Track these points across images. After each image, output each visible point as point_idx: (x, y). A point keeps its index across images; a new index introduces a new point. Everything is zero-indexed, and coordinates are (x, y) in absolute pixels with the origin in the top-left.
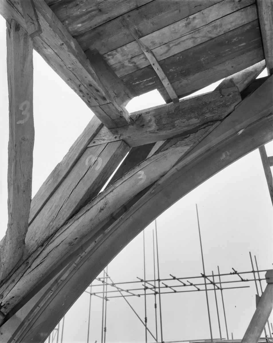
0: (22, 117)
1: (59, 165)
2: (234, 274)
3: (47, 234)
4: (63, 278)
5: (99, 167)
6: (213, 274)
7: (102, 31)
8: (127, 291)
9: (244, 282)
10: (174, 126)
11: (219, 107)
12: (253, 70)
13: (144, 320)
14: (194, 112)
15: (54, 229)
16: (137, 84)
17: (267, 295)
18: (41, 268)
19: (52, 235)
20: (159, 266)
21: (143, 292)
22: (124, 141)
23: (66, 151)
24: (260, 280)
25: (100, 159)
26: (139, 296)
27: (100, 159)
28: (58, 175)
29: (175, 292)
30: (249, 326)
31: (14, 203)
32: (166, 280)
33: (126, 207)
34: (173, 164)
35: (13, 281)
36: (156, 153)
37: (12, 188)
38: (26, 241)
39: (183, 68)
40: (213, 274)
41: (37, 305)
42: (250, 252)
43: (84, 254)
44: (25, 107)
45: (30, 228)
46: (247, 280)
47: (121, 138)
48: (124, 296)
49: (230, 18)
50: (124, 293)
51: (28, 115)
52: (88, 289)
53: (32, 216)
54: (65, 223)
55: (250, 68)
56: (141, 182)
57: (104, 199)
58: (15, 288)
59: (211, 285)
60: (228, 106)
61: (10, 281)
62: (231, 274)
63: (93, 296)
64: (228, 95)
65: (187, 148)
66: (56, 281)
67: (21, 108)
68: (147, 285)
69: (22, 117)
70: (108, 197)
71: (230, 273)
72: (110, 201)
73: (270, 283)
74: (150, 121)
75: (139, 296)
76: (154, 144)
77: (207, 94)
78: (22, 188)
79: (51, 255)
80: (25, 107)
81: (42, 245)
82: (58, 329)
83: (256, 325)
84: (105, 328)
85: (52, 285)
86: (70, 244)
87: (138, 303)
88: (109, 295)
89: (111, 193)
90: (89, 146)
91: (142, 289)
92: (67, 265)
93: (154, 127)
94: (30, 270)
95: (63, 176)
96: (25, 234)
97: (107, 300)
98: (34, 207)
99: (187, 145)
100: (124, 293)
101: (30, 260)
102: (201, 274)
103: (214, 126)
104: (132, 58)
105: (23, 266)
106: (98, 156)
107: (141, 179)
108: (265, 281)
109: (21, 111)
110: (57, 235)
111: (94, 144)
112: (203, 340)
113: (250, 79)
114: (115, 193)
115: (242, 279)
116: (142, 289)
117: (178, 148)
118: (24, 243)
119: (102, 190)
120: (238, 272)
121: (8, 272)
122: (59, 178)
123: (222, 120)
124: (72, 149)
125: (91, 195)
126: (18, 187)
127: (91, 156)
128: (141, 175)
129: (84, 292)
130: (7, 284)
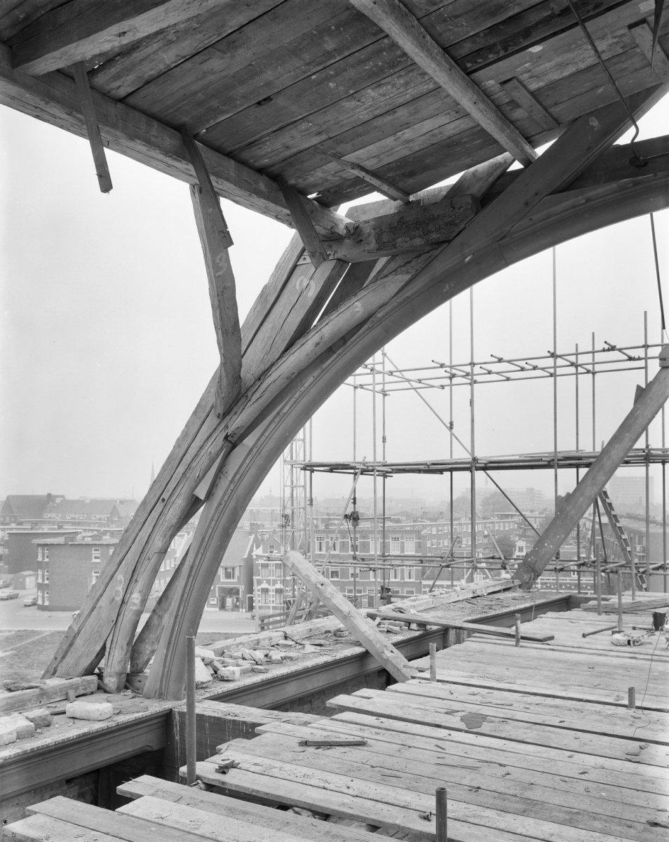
0: (219, 269)
1: (265, 287)
2: (609, 350)
3: (263, 368)
4: (284, 411)
5: (312, 293)
8: (420, 381)
10: (395, 246)
11: (446, 224)
12: (502, 161)
13: (449, 425)
14: (418, 229)
15: (270, 363)
16: (350, 192)
17: (656, 386)
18: (260, 401)
19: (268, 369)
21: (447, 382)
22: (339, 260)
23: (271, 269)
25: (312, 283)
26: (443, 387)
27: (312, 283)
28: (266, 300)
29: (508, 379)
30: (616, 432)
31: (224, 345)
33: (343, 340)
34: (392, 295)
35: (236, 413)
36: (372, 282)
37: (220, 331)
38: (242, 376)
39: (401, 176)
41: (262, 434)
42: (645, 313)
43: (303, 388)
44: (221, 260)
45: (244, 360)
46: (639, 357)
47: (336, 257)
48: (415, 389)
49: (452, 125)
50: (416, 385)
51: (226, 265)
52: (350, 380)
53: (244, 348)
54: (280, 357)
55: (499, 158)
56: (359, 315)
57: (320, 332)
59: (571, 367)
60: (456, 225)
61: (232, 413)
62: (604, 350)
63: (359, 390)
64: (461, 207)
65: (407, 277)
66: (278, 413)
67: (218, 261)
68: (454, 371)
69: (219, 269)
70: (323, 330)
71: (601, 349)
72: (326, 336)
73: (666, 367)
74: (369, 235)
75: (443, 387)
76: (375, 262)
77: (350, 331)
78: (230, 330)
79: (270, 389)
80: (221, 260)
81: (259, 379)
82: (304, 440)
83: (628, 431)
85: (275, 417)
86: (288, 378)
87: (438, 398)
88: (387, 387)
89: (327, 326)
90: (298, 264)
92: (335, 290)
93: (373, 245)
95: (272, 301)
96: (240, 370)
97: (385, 395)
98: (246, 336)
99: (408, 273)
100: (416, 385)
101: (249, 394)
102: (549, 352)
103: (439, 250)
104: (335, 173)
105: (243, 399)
106: (311, 279)
107: (358, 312)
108: (658, 360)
109: (218, 263)
110: (274, 369)
111: (304, 262)
112: (546, 453)
113: (499, 172)
114: (327, 329)
115: (628, 356)
117: (398, 276)
118: (241, 378)
119: (315, 323)
120: (618, 347)
121: (228, 405)
122: (270, 301)
123: (449, 242)
124: (278, 267)
125: (303, 329)
126: (226, 331)
127: (302, 277)
128: (356, 307)
129: (342, 385)
130: (230, 417)
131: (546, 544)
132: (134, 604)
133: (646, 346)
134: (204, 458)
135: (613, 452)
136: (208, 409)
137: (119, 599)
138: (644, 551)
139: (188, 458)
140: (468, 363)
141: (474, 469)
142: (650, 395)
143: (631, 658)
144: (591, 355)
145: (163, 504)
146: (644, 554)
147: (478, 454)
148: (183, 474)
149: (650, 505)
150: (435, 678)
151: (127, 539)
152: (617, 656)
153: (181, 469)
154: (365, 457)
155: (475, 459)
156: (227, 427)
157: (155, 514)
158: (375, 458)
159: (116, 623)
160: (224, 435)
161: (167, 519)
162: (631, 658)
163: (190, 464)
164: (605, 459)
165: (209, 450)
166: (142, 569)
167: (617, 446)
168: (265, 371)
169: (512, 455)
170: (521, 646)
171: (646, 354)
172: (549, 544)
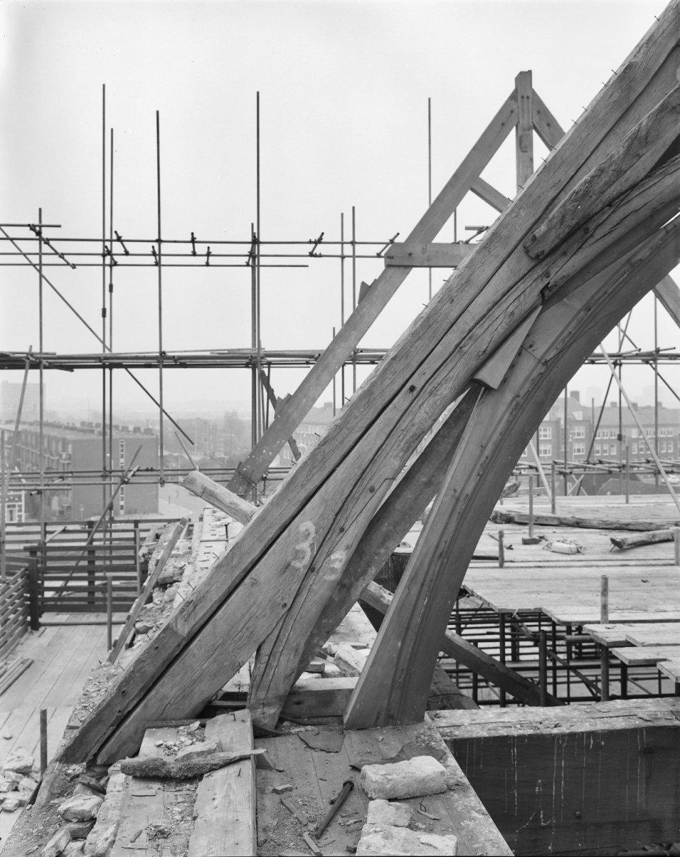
6: (101, 265)
7: (89, 405)
9: (313, 258)
17: (381, 284)
19: (627, 191)
20: (144, 392)
24: (209, 254)
32: (664, 381)
40: (101, 265)
58: (570, 263)
83: (354, 329)
84: (111, 287)
91: (214, 255)
94: (592, 240)
101: (592, 226)
110: (636, 193)
112: (225, 350)
115: (63, 258)
116: (214, 255)
131: (264, 451)
132: (333, 570)
133: (353, 243)
134: (499, 321)
135: (339, 350)
136: (514, 243)
137: (301, 565)
138: (70, 459)
139: (467, 321)
140: (155, 239)
141: (161, 366)
142: (376, 294)
143: (622, 566)
144: (340, 245)
145: (411, 397)
146: (69, 462)
147: (661, 346)
148: (457, 346)
149: (44, 413)
150: (607, 619)
151: (324, 460)
152: (609, 566)
153: (453, 338)
154: (31, 347)
155: (162, 353)
156: (547, 274)
157: (391, 414)
158: (41, 349)
159: (290, 609)
160: (541, 286)
161: (416, 421)
162: (622, 566)
163: (470, 331)
164: (330, 358)
165: (511, 309)
166: (357, 509)
167: (343, 345)
168: (622, 194)
169: (185, 351)
170: (506, 567)
171: (40, 261)
172: (268, 451)
